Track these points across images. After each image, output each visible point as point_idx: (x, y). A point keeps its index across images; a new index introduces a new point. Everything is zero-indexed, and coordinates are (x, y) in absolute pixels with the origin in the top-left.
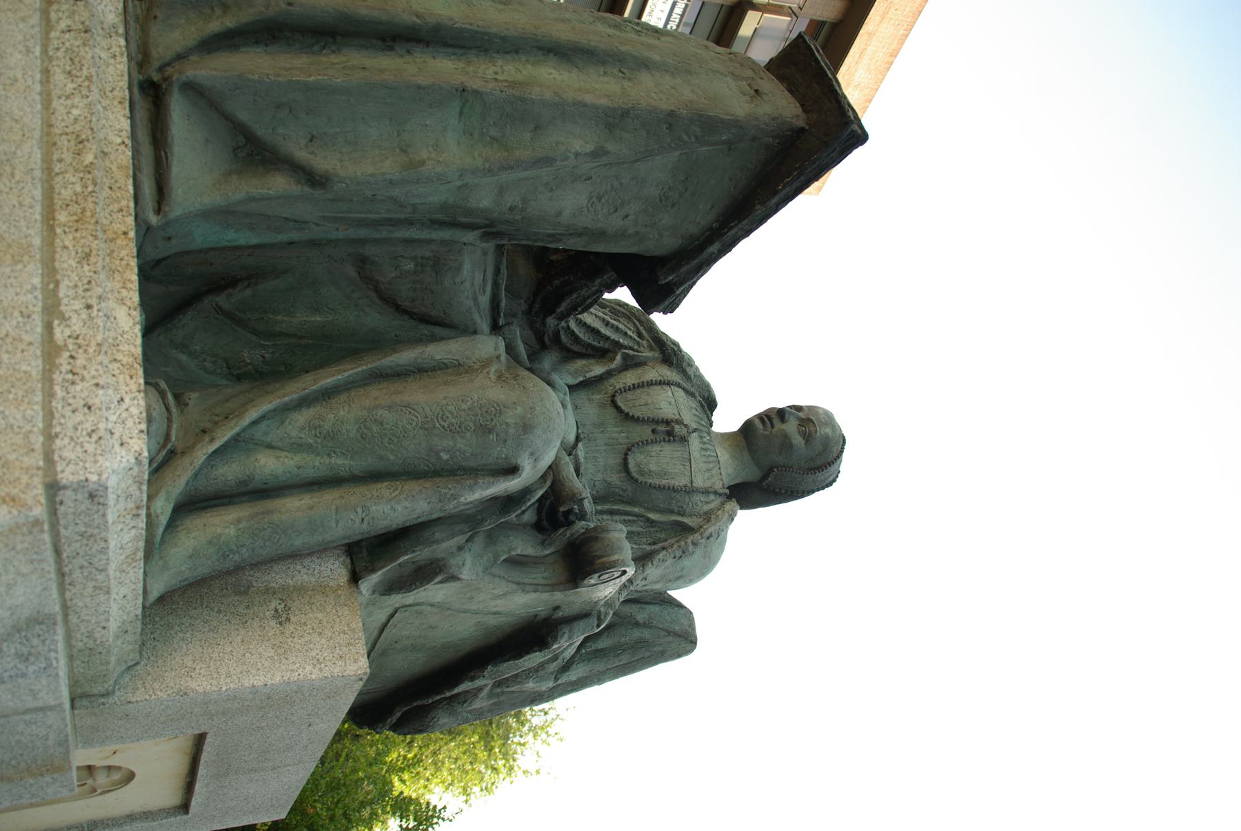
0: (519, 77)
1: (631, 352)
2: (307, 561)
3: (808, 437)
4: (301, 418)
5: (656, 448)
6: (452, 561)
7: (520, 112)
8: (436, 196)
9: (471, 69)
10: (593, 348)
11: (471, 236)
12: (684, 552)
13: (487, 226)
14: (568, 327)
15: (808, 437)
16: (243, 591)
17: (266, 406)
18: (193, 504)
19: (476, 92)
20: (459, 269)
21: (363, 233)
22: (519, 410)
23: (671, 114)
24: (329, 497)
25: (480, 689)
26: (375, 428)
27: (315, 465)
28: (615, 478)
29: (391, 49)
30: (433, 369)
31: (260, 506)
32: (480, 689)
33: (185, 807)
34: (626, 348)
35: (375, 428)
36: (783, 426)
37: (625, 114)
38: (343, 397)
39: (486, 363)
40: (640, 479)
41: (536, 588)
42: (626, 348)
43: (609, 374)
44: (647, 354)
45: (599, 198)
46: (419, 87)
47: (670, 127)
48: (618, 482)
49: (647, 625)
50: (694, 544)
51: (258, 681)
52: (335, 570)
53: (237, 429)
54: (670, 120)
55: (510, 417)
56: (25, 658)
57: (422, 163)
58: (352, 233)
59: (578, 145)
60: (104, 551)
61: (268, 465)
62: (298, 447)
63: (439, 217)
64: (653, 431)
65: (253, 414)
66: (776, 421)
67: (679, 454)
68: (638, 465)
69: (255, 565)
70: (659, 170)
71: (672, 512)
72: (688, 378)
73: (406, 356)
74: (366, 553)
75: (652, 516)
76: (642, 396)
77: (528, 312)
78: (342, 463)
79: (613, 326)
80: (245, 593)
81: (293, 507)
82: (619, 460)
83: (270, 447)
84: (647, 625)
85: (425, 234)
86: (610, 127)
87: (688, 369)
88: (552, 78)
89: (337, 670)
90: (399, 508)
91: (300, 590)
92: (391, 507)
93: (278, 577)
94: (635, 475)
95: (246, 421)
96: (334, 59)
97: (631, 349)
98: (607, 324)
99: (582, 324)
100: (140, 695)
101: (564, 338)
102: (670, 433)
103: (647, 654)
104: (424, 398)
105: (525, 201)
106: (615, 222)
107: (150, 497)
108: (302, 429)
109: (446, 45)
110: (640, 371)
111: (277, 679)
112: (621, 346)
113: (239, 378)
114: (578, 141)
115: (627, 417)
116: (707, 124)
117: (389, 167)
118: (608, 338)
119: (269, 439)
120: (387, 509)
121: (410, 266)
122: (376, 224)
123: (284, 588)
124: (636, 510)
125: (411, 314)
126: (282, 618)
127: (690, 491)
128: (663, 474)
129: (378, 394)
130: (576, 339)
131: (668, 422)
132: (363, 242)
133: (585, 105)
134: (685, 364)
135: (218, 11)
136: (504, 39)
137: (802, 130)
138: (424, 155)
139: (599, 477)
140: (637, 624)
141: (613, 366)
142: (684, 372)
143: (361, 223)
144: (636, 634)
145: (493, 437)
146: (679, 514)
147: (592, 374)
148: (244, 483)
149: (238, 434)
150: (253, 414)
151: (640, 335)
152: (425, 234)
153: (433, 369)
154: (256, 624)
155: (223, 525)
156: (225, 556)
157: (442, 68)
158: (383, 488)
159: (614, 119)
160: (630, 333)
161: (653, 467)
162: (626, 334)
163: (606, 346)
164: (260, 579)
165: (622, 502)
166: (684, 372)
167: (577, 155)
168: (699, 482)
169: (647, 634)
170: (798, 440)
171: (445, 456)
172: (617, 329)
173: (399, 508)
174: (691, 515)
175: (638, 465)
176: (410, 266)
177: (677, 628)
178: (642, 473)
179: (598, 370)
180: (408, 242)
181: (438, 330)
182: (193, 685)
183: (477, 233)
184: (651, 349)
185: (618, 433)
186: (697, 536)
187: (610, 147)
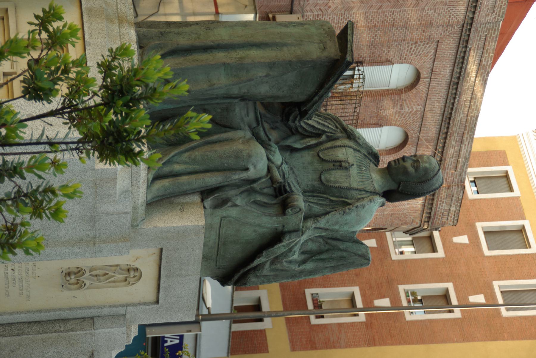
0: (244, 55)
1: (330, 134)
2: (189, 196)
3: (417, 169)
4: (186, 155)
5: (334, 172)
6: (233, 198)
7: (241, 67)
8: (222, 92)
9: (229, 55)
10: (314, 133)
11: (236, 101)
12: (344, 212)
13: (241, 97)
14: (301, 126)
15: (417, 169)
16: (172, 203)
17: (176, 151)
18: (157, 178)
19: (228, 64)
20: (234, 110)
21: (203, 102)
22: (247, 151)
23: (290, 61)
24: (193, 177)
25: (264, 264)
26: (206, 157)
27: (190, 168)
28: (316, 183)
29: (206, 52)
30: (224, 141)
31: (175, 178)
32: (264, 264)
33: (157, 302)
34: (329, 133)
35: (206, 157)
36: (405, 164)
37: (274, 63)
38: (197, 149)
39: (240, 138)
40: (326, 184)
41: (270, 215)
42: (329, 133)
43: (320, 143)
44: (340, 135)
45: (273, 87)
46: (212, 65)
47: (290, 65)
48: (318, 185)
49: (345, 251)
50: (349, 209)
51: (175, 225)
52: (197, 198)
53: (168, 158)
54: (290, 63)
55: (244, 153)
56: (125, 198)
57: (214, 84)
58: (199, 103)
59: (260, 74)
60: (140, 176)
61: (177, 168)
62: (185, 163)
63: (225, 96)
64: (334, 165)
65: (173, 154)
66: (401, 162)
67: (345, 174)
68: (326, 178)
69: (175, 196)
70: (291, 77)
71: (342, 197)
72: (359, 144)
73: (215, 137)
74: (206, 193)
75: (332, 198)
76: (332, 152)
77: (282, 121)
78: (197, 167)
79: (322, 124)
80: (172, 204)
81: (184, 179)
82: (318, 177)
83: (178, 163)
84: (345, 251)
85: (222, 101)
86: (270, 68)
87: (358, 140)
88: (255, 54)
89: (196, 224)
90: (213, 179)
91: (187, 203)
92: (212, 180)
93: (181, 200)
94: (325, 182)
95: (171, 156)
96: (190, 57)
97: (331, 133)
98: (319, 123)
99: (306, 123)
100: (145, 227)
101: (300, 130)
102: (341, 166)
103: (345, 263)
104: (219, 149)
105: (248, 90)
106: (280, 93)
107: (148, 174)
108: (186, 158)
109: (222, 48)
110: (334, 142)
111: (180, 225)
112: (325, 132)
113: (170, 145)
114: (260, 73)
115: (323, 160)
116: (302, 63)
117: (205, 86)
118: (319, 129)
119: (177, 161)
120: (210, 179)
121: (219, 110)
122: (206, 100)
123: (183, 203)
124: (325, 196)
125: (221, 125)
126: (182, 210)
127: (350, 189)
128: (336, 182)
129: (207, 148)
130: (306, 130)
131: (340, 162)
132: (204, 105)
133: (261, 63)
134: (356, 139)
135: (160, 49)
136: (239, 45)
137: (338, 60)
138: (215, 82)
139: (310, 183)
140: (340, 250)
141: (321, 140)
142: (356, 142)
143: (202, 100)
144: (340, 254)
145: (240, 159)
146: (345, 198)
147: (310, 144)
148: (170, 172)
149: (169, 159)
150: (173, 154)
151: (337, 127)
152: (222, 101)
153: (224, 141)
154: (175, 211)
155: (166, 182)
156: (166, 190)
157: (221, 56)
158: (209, 174)
159: (272, 65)
160: (330, 126)
161: (332, 179)
162: (328, 127)
163: (320, 132)
164: (176, 200)
165: (321, 193)
166: (356, 142)
167: (260, 77)
168: (355, 185)
169: (345, 254)
170: (411, 170)
171: (226, 165)
172: (324, 125)
173: (213, 179)
174: (351, 199)
175: (326, 178)
176: (219, 110)
177: (360, 253)
178: (327, 181)
179: (313, 142)
180: (218, 104)
181: (228, 129)
182: (158, 225)
183: (239, 99)
184: (342, 132)
185: (319, 166)
186: (351, 206)
187: (271, 73)
